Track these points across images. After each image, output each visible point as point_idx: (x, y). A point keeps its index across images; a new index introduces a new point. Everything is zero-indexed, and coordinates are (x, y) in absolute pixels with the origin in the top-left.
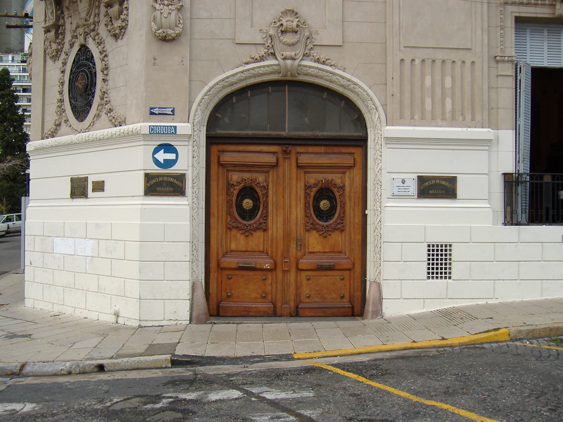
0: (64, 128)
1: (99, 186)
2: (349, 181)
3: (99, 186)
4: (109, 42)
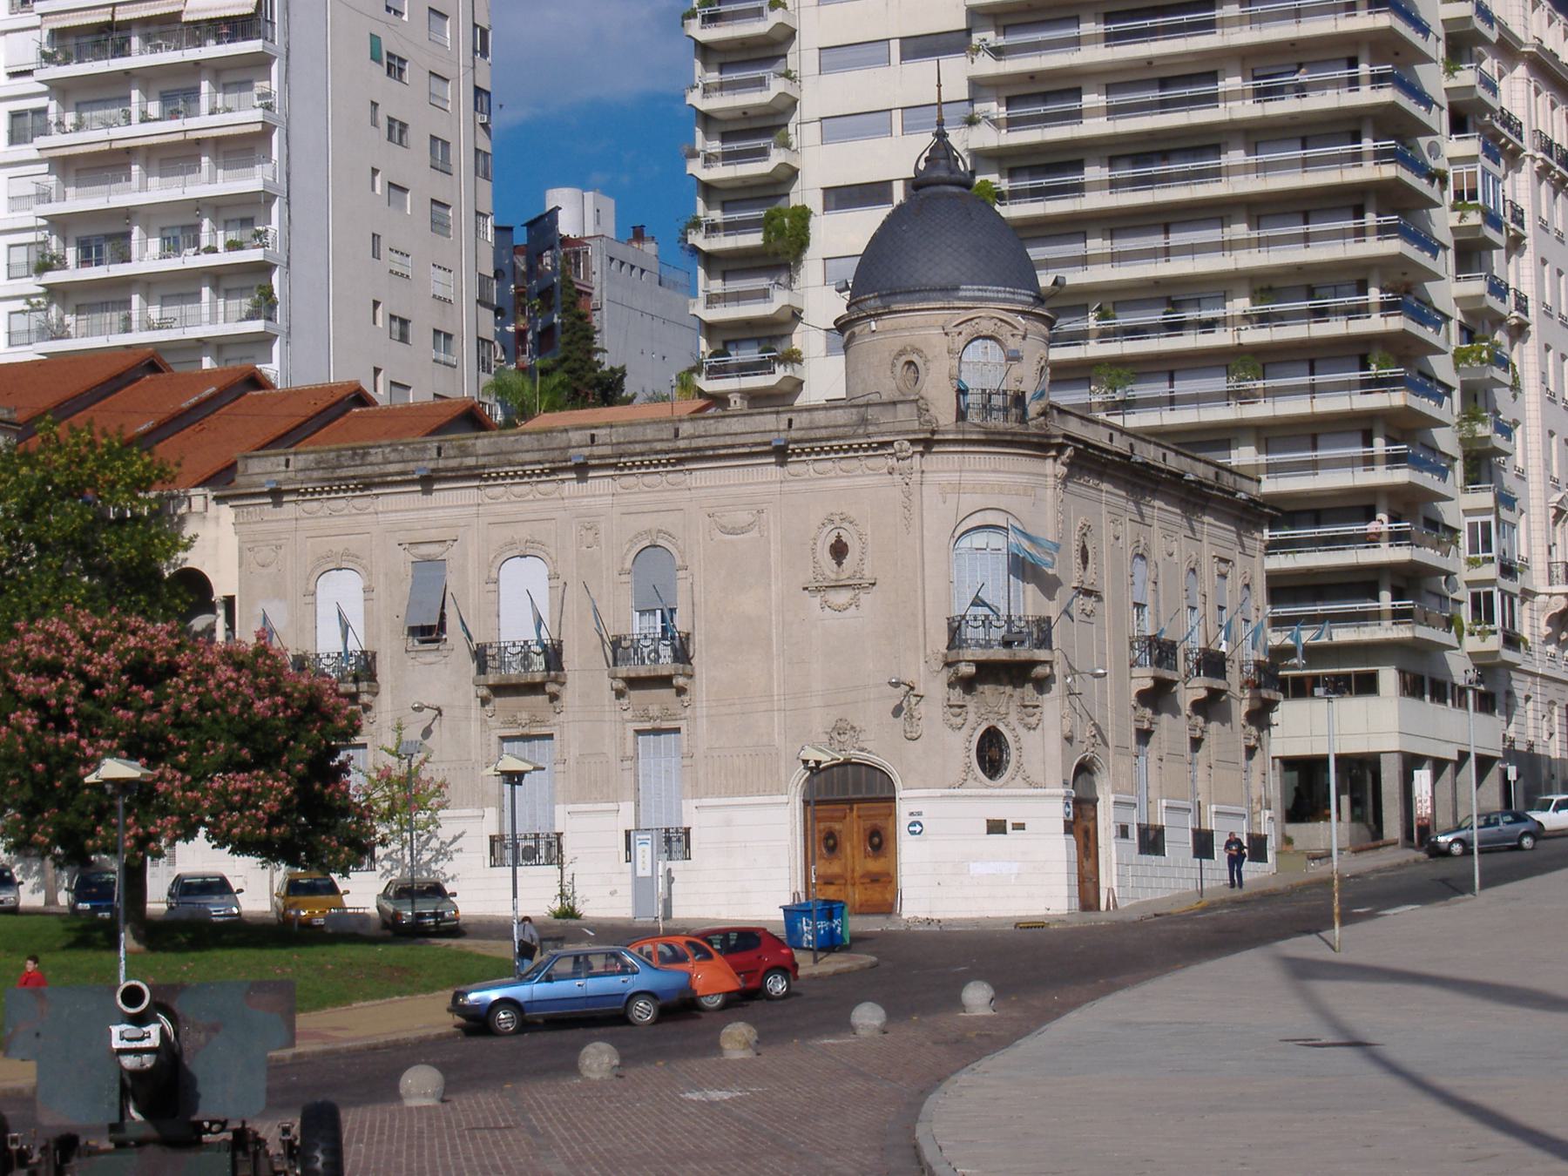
0: (970, 782)
1: (1020, 827)
2: (1091, 825)
3: (1020, 827)
4: (1021, 731)
